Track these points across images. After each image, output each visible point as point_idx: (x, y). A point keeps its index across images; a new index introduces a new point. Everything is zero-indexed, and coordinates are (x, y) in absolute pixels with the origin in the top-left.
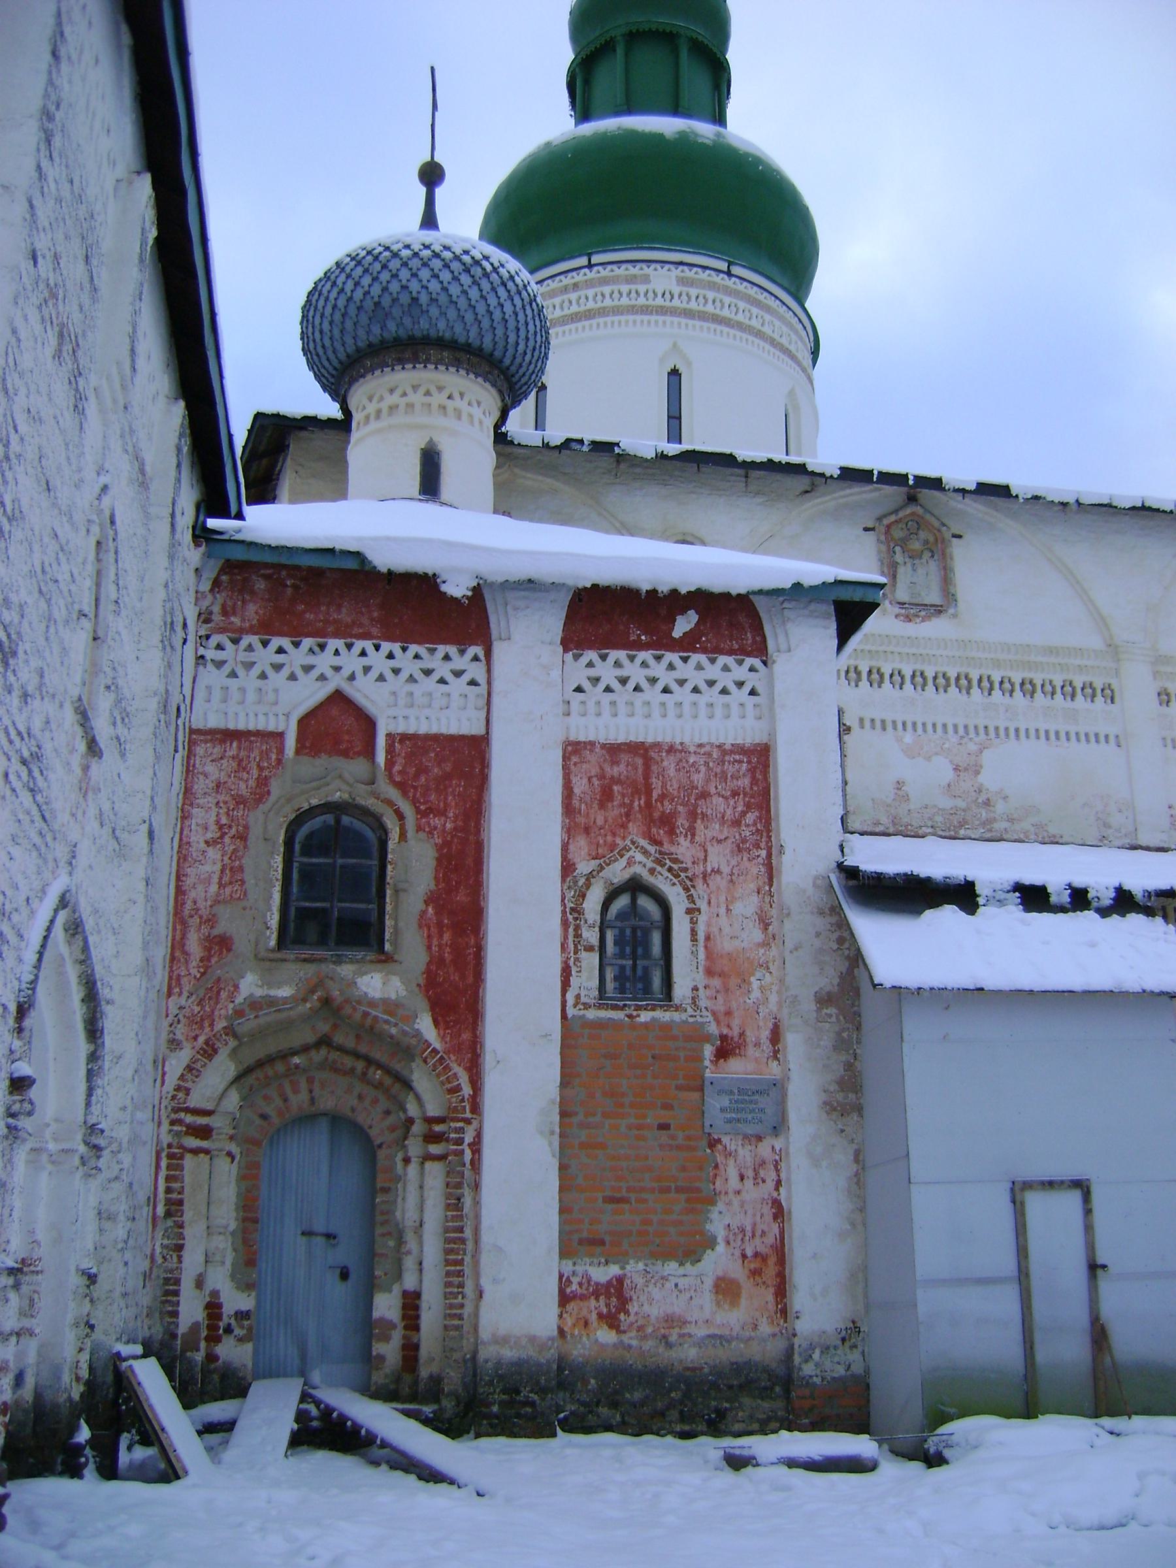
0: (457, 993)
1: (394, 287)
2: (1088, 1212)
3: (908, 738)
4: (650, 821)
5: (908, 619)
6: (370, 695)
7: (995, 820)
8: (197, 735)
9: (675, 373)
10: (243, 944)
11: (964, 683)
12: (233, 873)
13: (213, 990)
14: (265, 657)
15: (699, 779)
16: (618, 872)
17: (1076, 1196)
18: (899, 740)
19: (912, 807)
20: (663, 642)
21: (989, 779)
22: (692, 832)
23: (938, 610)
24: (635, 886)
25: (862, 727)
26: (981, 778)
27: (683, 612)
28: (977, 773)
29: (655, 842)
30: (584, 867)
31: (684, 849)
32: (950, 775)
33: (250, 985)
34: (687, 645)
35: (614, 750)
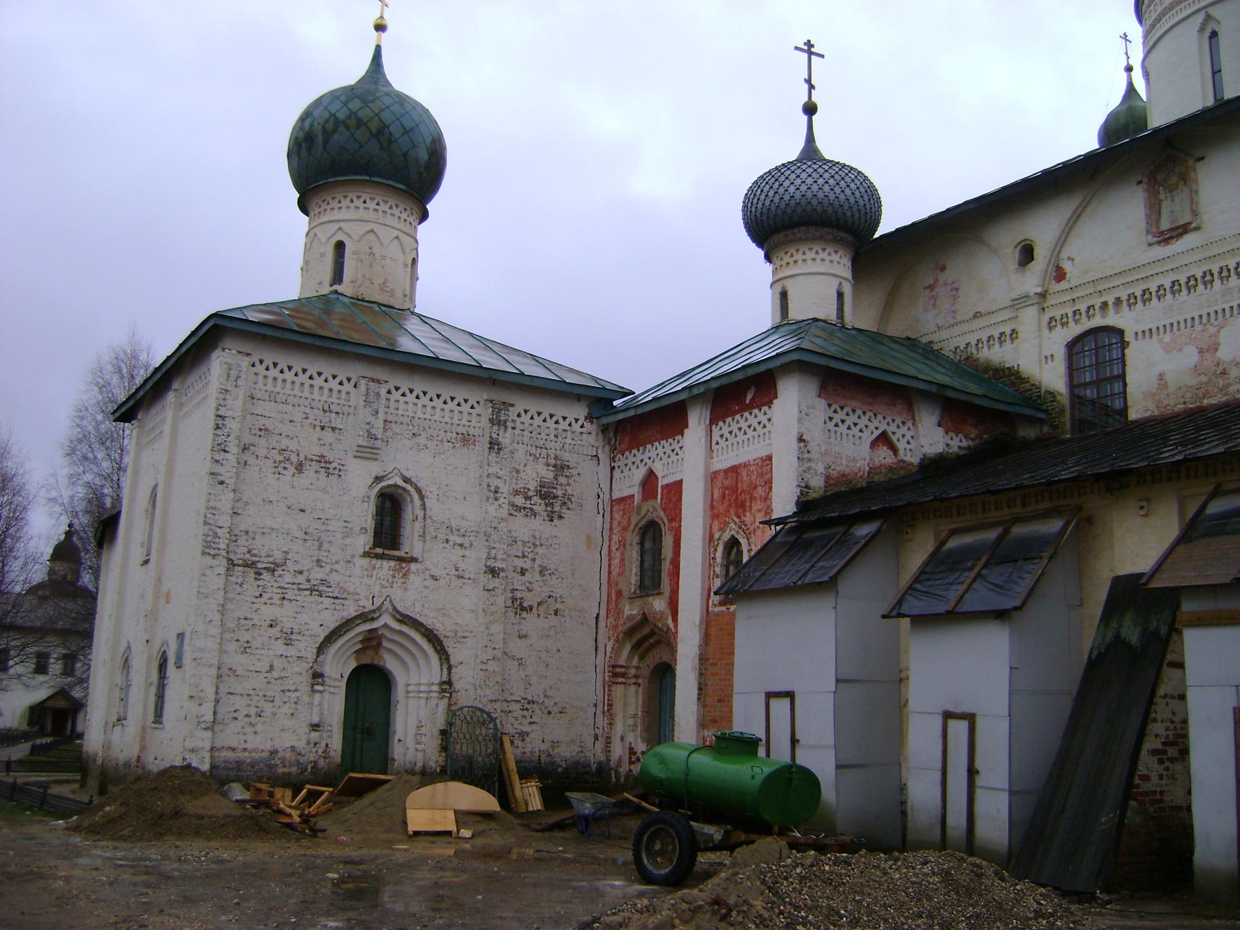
1: (815, 187)
2: (792, 709)
3: (1167, 338)
5: (1166, 241)
7: (1229, 384)
8: (614, 502)
10: (626, 594)
11: (1207, 279)
13: (619, 612)
17: (787, 701)
18: (1160, 341)
19: (1170, 391)
21: (1224, 354)
23: (1182, 230)
25: (1137, 339)
26: (1219, 354)
27: (749, 388)
28: (1216, 350)
29: (739, 517)
30: (717, 536)
34: (749, 408)
35: (727, 471)
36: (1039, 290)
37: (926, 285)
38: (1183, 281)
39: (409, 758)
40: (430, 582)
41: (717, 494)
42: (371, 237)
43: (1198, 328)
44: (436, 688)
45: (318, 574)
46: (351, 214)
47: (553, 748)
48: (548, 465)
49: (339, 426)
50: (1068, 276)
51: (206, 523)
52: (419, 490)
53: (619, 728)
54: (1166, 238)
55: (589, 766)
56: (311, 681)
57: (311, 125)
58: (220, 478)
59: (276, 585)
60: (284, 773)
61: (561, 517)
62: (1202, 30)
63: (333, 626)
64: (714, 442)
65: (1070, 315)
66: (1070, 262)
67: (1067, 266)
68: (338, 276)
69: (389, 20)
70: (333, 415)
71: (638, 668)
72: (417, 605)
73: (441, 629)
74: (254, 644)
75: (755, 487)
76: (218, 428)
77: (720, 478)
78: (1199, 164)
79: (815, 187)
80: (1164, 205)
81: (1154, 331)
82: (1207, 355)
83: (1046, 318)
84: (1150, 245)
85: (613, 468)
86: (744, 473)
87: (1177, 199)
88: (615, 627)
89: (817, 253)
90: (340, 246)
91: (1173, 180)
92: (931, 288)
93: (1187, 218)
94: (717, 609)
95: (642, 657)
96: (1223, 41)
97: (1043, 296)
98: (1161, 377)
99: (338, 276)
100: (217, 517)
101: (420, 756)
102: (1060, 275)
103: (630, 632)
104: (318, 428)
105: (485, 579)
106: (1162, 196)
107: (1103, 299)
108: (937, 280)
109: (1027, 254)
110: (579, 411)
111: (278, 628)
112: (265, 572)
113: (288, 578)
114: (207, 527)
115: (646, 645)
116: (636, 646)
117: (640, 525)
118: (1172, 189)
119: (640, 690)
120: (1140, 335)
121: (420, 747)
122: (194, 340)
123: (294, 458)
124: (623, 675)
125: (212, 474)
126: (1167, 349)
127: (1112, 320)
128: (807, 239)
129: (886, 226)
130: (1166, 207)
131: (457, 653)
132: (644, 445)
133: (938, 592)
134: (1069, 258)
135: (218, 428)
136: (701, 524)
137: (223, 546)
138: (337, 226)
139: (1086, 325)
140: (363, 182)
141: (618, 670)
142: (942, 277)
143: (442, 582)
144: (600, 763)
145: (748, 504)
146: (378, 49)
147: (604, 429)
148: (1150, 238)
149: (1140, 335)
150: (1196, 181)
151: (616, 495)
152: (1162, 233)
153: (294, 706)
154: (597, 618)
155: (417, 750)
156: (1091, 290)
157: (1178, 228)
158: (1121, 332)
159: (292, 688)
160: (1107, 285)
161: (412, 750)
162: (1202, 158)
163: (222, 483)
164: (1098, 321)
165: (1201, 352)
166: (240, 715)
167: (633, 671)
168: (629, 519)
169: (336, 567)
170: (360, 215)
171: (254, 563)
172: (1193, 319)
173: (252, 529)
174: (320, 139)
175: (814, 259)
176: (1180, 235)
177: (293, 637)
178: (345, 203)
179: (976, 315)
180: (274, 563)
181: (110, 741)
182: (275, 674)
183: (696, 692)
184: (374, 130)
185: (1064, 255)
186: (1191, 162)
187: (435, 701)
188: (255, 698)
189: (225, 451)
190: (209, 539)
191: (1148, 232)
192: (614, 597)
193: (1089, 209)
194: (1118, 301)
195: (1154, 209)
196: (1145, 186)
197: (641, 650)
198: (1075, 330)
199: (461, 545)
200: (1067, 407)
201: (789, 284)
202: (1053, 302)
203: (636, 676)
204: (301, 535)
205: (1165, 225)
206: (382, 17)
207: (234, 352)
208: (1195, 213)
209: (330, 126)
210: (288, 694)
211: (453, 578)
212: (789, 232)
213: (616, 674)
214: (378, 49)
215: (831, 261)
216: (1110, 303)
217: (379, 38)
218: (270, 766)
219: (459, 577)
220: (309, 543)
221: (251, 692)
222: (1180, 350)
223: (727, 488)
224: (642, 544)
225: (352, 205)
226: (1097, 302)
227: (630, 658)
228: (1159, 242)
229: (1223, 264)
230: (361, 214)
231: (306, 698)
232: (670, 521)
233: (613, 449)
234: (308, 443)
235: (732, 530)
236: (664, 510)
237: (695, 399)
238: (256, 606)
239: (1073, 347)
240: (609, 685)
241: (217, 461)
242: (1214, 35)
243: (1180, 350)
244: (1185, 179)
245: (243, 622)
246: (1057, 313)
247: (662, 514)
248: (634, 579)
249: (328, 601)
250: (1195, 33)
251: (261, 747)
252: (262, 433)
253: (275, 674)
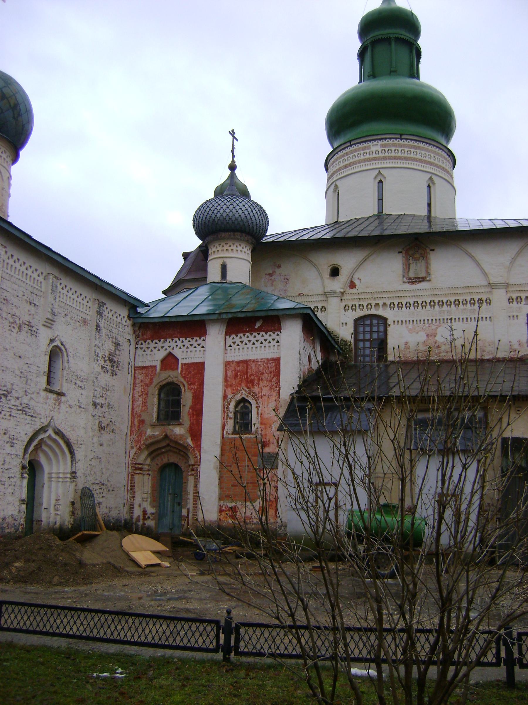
0: (196, 433)
3: (411, 326)
4: (247, 382)
5: (413, 283)
6: (177, 353)
8: (136, 368)
9: (380, 182)
10: (147, 422)
11: (432, 304)
12: (145, 404)
13: (141, 434)
15: (261, 369)
16: (238, 397)
18: (407, 327)
20: (252, 330)
22: (258, 384)
23: (422, 279)
24: (243, 400)
26: (436, 338)
28: (435, 336)
29: (248, 388)
30: (230, 396)
31: (256, 389)
32: (425, 338)
33: (149, 432)
34: (259, 331)
35: (238, 363)
36: (342, 291)
37: (267, 272)
38: (420, 303)
39: (52, 520)
40: (68, 409)
41: (229, 373)
43: (427, 325)
45: (25, 400)
47: (110, 511)
48: (113, 342)
49: (37, 304)
50: (357, 287)
53: (138, 500)
54: (414, 281)
55: (121, 522)
60: (8, 532)
61: (116, 374)
62: (375, 178)
63: (31, 434)
64: (228, 345)
65: (357, 306)
66: (359, 281)
67: (357, 282)
71: (149, 465)
72: (63, 423)
73: (72, 439)
75: (262, 373)
77: (233, 365)
78: (431, 252)
80: (411, 266)
81: (404, 322)
82: (430, 338)
83: (343, 304)
84: (404, 282)
85: (136, 348)
86: (253, 366)
87: (419, 265)
88: (138, 441)
91: (417, 256)
92: (271, 275)
93: (423, 274)
94: (230, 436)
95: (153, 459)
96: (385, 186)
97: (343, 293)
98: (406, 343)
101: (58, 518)
102: (352, 285)
103: (148, 446)
104: (29, 303)
105: (91, 408)
106: (411, 261)
107: (377, 302)
108: (274, 272)
109: (335, 272)
110: (124, 312)
111: (7, 436)
113: (13, 402)
115: (159, 452)
116: (150, 454)
117: (161, 384)
118: (416, 260)
119: (150, 478)
120: (396, 322)
123: (18, 322)
124: (141, 469)
126: (410, 331)
127: (380, 312)
128: (241, 240)
129: (264, 240)
130: (413, 267)
131: (79, 454)
132: (165, 339)
133: (413, 443)
134: (358, 279)
136: (221, 390)
139: (366, 312)
142: (278, 271)
143: (73, 409)
144: (125, 520)
145: (256, 381)
147: (134, 325)
148: (405, 280)
149: (396, 322)
150: (429, 259)
152: (410, 278)
155: (57, 514)
156: (370, 296)
157: (419, 278)
158: (385, 319)
160: (379, 296)
161: (52, 516)
162: (433, 250)
164: (373, 312)
165: (427, 336)
167: (146, 467)
169: (33, 396)
172: (424, 320)
176: (420, 282)
177: (15, 441)
179: (299, 295)
180: (7, 391)
182: (6, 466)
183: (218, 481)
184: (12, 104)
185: (356, 276)
186: (428, 251)
187: (68, 484)
191: (404, 276)
192: (136, 423)
193: (371, 258)
194: (385, 304)
195: (407, 267)
196: (404, 255)
197: (153, 455)
198: (360, 313)
199: (81, 387)
200: (353, 349)
201: (228, 262)
202: (348, 298)
203: (149, 470)
204: (18, 373)
205: (412, 275)
208: (428, 273)
210: (11, 479)
211: (78, 407)
212: (232, 233)
213: (137, 468)
215: (237, 250)
216: (380, 305)
219: (80, 407)
222: (417, 333)
224: (159, 394)
226: (373, 303)
227: (146, 459)
228: (409, 282)
229: (440, 299)
231: (18, 483)
232: (189, 385)
233: (137, 337)
234: (24, 312)
235: (243, 394)
236: (184, 378)
239: (358, 321)
242: (380, 182)
243: (417, 333)
244: (424, 256)
246: (350, 304)
248: (155, 415)
249: (29, 418)
250: (373, 179)
252: (5, 302)
253: (6, 466)
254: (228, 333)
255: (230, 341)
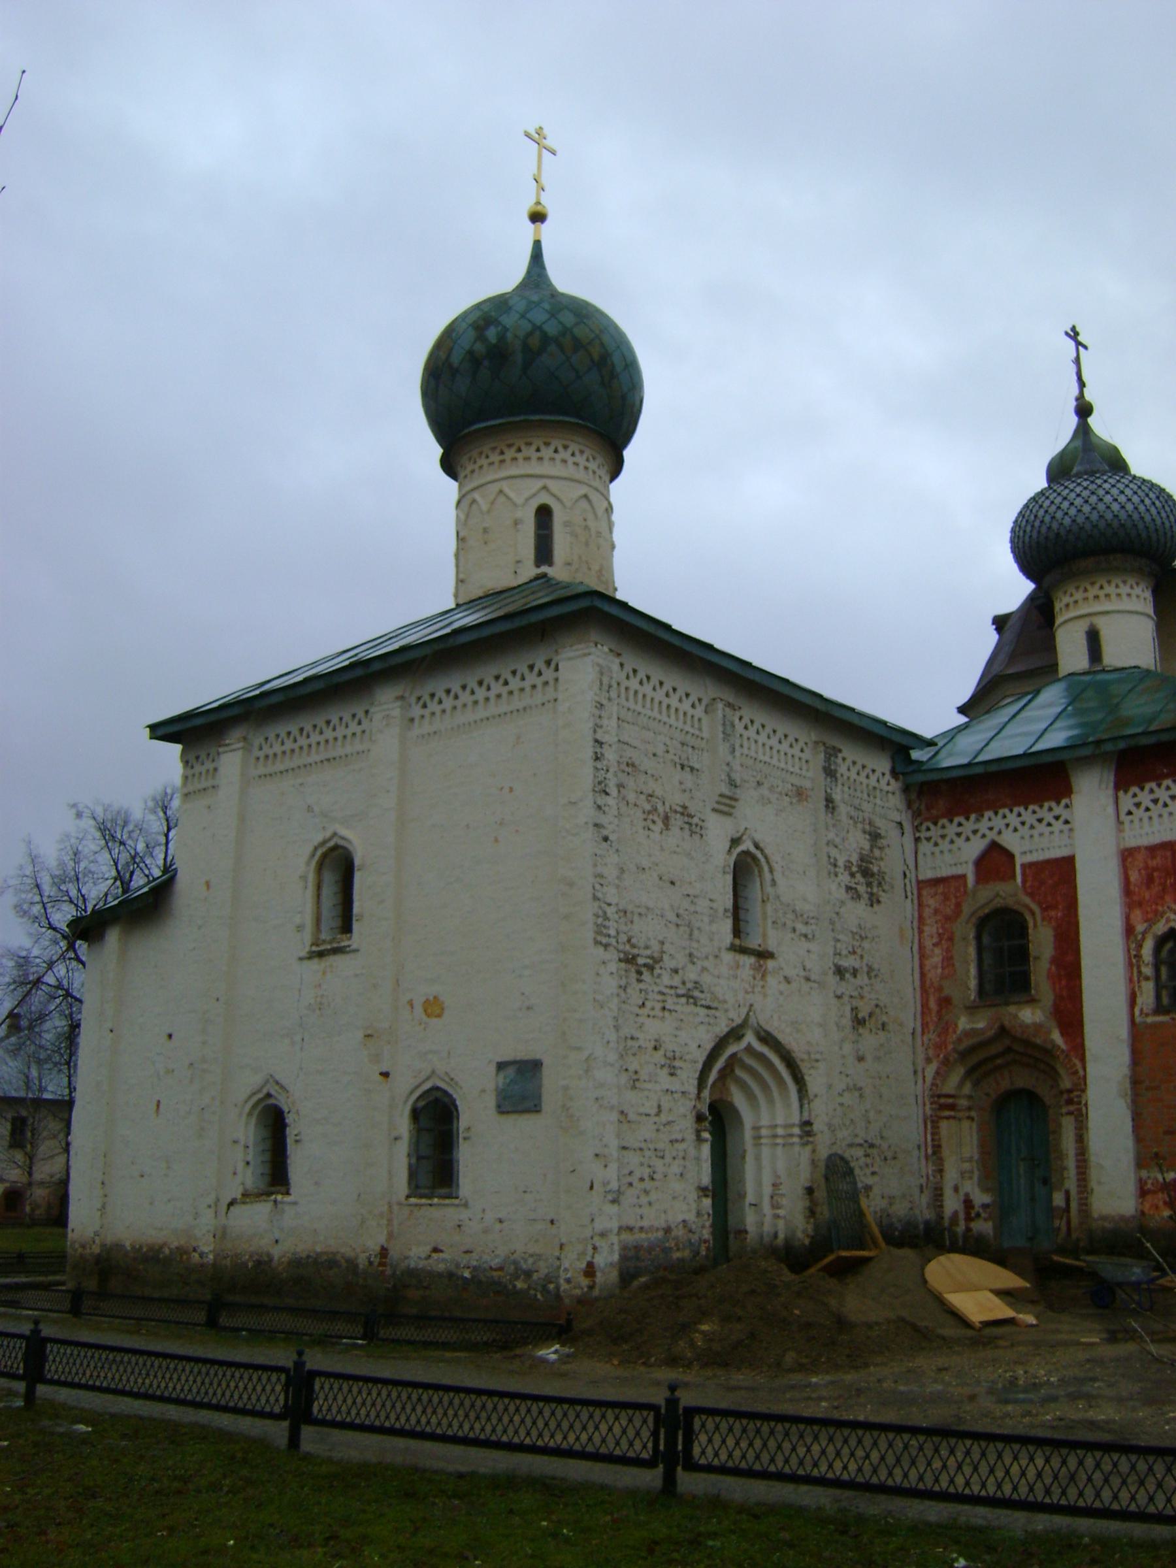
0: (1070, 1016)
6: (1009, 841)
13: (945, 1028)
14: (952, 829)
30: (1140, 928)
35: (1152, 850)
39: (767, 1228)
41: (1134, 876)
42: (584, 504)
44: (797, 1131)
46: (557, 470)
47: (891, 1204)
51: (595, 898)
52: (766, 857)
53: (951, 1175)
56: (695, 1126)
57: (502, 337)
58: (605, 832)
59: (656, 989)
68: (544, 553)
69: (549, 204)
70: (690, 750)
71: (970, 1097)
74: (643, 1075)
76: (597, 759)
77: (1140, 859)
79: (1059, 515)
89: (1132, 587)
90: (544, 514)
94: (1150, 1020)
99: (544, 553)
100: (605, 889)
101: (781, 1224)
103: (964, 1055)
104: (679, 767)
111: (661, 1052)
112: (643, 969)
113: (666, 979)
114: (596, 904)
116: (969, 1073)
119: (974, 1126)
121: (781, 1212)
122: (651, 629)
123: (660, 809)
124: (952, 1107)
125: (596, 825)
131: (815, 1081)
135: (597, 759)
137: (612, 932)
138: (540, 483)
140: (542, 424)
141: (942, 1101)
146: (537, 245)
147: (906, 789)
151: (927, 874)
153: (682, 1162)
154: (913, 1034)
159: (679, 1137)
161: (768, 1220)
163: (606, 839)
166: (634, 1179)
167: (963, 1102)
168: (958, 905)
170: (542, 470)
171: (634, 957)
173: (630, 908)
174: (519, 358)
175: (1096, 597)
178: (547, 452)
180: (652, 957)
181: (224, 1228)
184: (596, 357)
187: (797, 1148)
188: (647, 1153)
189: (607, 794)
190: (600, 921)
199: (806, 936)
201: (1102, 624)
203: (969, 1109)
206: (538, 203)
207: (606, 649)
209: (535, 342)
210: (676, 1145)
213: (942, 1106)
214: (537, 245)
217: (537, 232)
218: (666, 1251)
220: (682, 928)
221: (643, 1145)
223: (1155, 869)
224: (978, 938)
225: (520, 456)
227: (961, 1084)
230: (570, 471)
231: (692, 1152)
232: (1044, 910)
233: (916, 814)
237: (1087, 761)
238: (640, 1019)
240: (932, 1122)
241: (599, 807)
245: (630, 1043)
247: (1027, 900)
251: (656, 1224)
252: (630, 770)
253: (664, 1118)
254: (1121, 784)
255: (1126, 801)
